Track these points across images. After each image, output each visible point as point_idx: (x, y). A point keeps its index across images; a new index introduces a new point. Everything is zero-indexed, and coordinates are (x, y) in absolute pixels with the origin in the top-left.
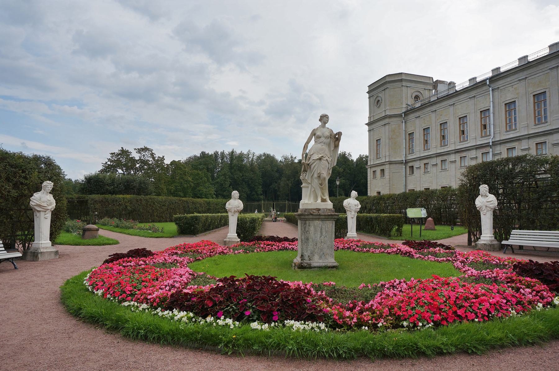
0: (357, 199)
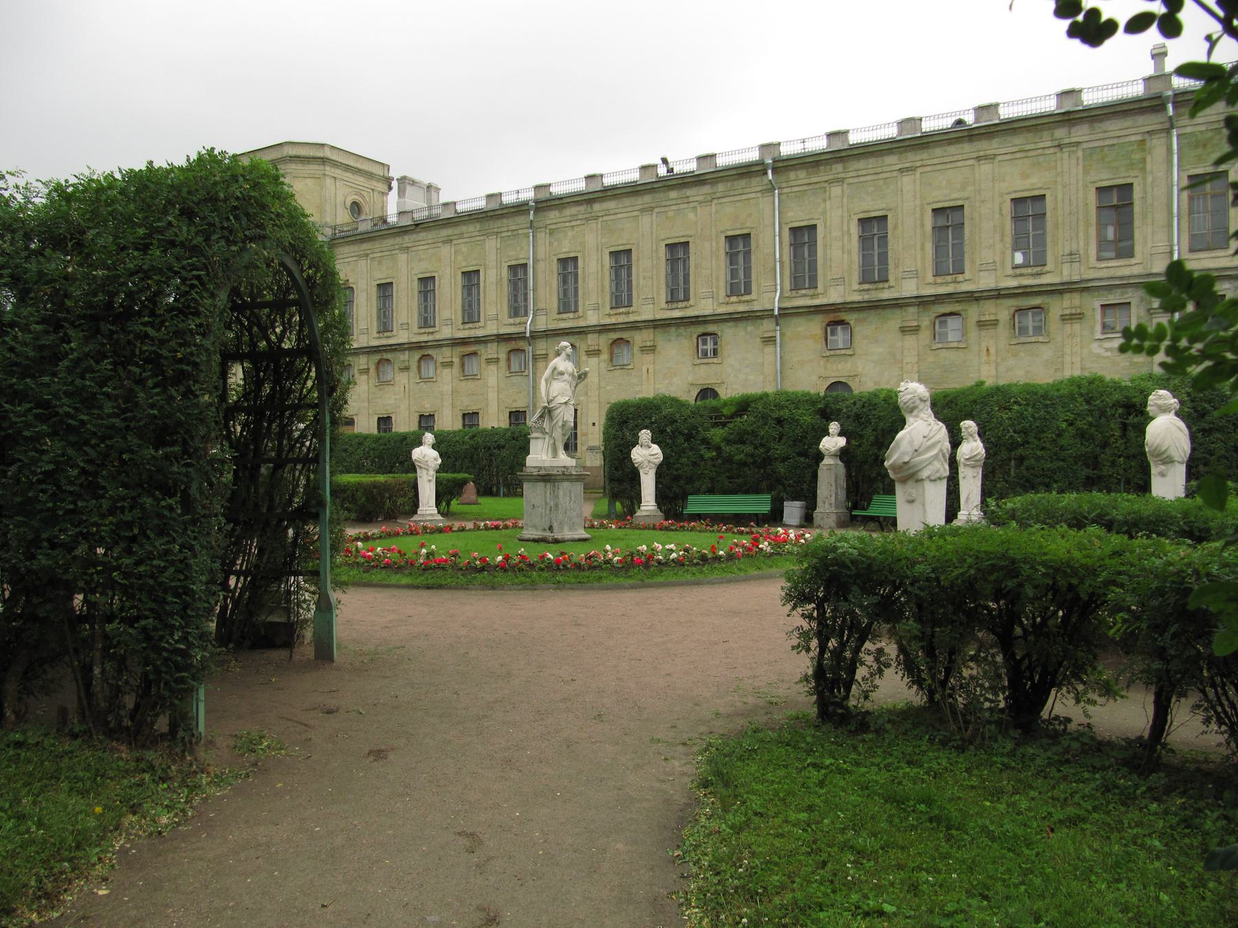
0: (434, 447)
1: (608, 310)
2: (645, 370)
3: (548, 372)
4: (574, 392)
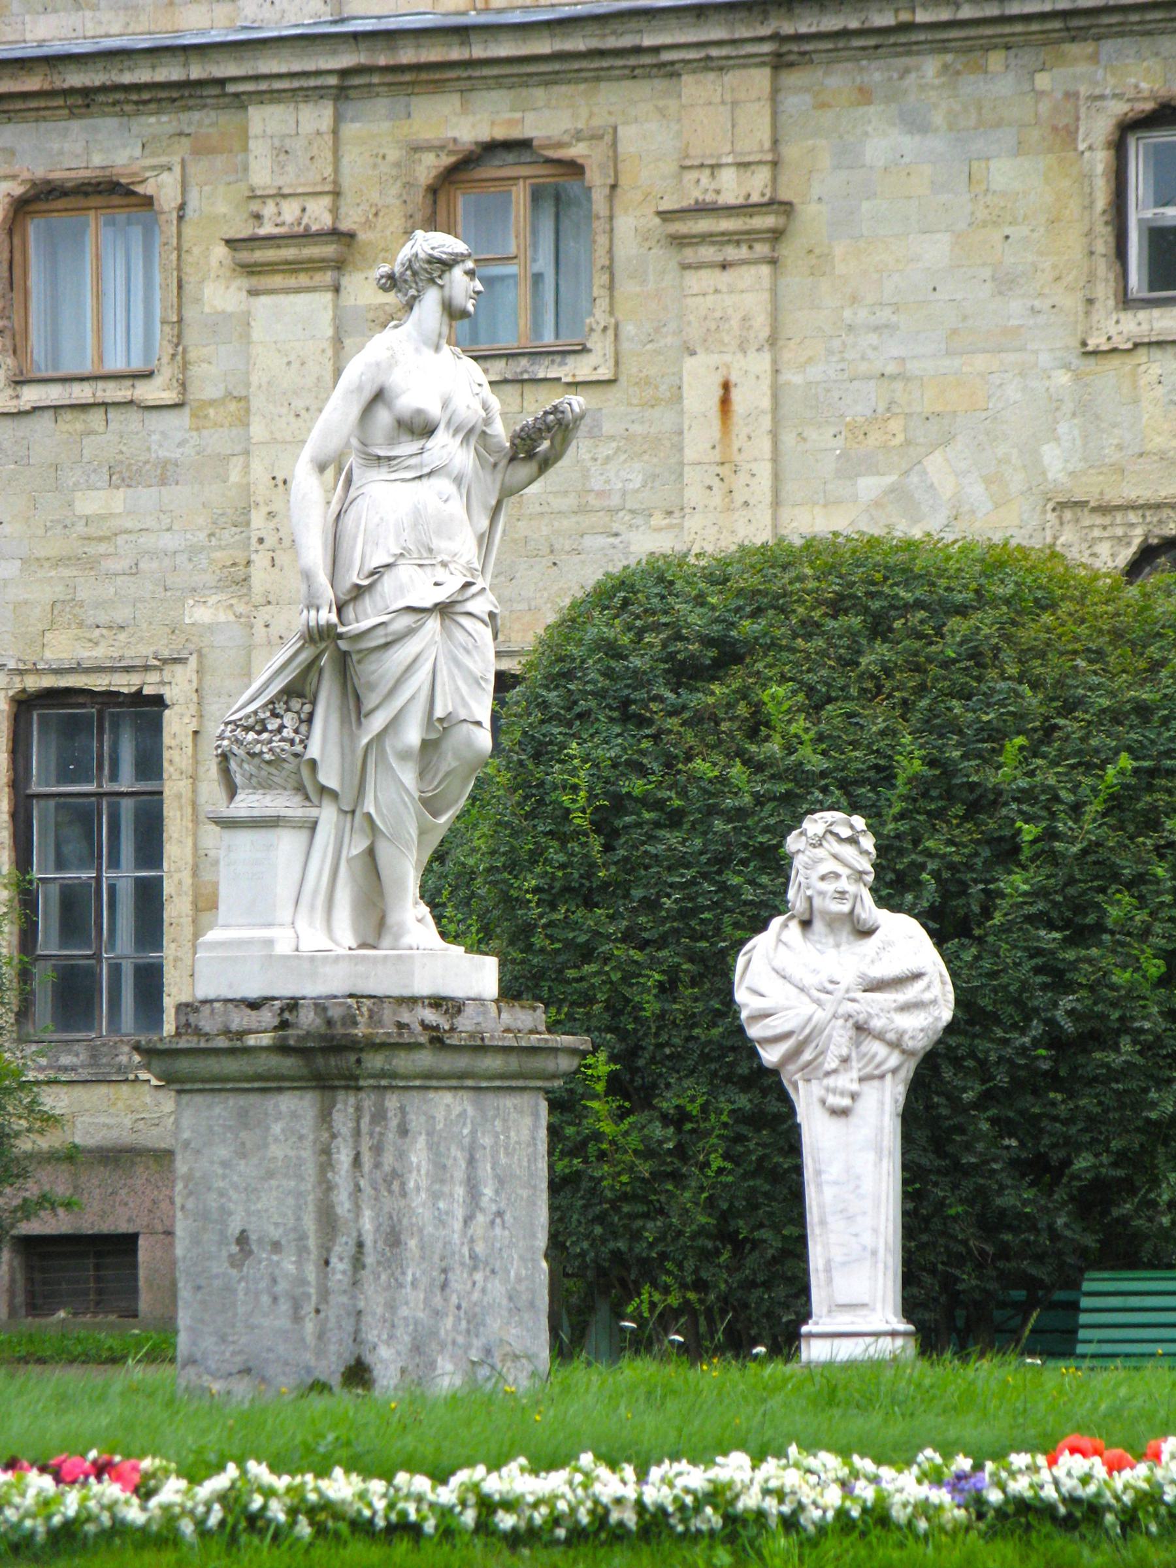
2: (700, 398)
3: (337, 414)
4: (485, 540)
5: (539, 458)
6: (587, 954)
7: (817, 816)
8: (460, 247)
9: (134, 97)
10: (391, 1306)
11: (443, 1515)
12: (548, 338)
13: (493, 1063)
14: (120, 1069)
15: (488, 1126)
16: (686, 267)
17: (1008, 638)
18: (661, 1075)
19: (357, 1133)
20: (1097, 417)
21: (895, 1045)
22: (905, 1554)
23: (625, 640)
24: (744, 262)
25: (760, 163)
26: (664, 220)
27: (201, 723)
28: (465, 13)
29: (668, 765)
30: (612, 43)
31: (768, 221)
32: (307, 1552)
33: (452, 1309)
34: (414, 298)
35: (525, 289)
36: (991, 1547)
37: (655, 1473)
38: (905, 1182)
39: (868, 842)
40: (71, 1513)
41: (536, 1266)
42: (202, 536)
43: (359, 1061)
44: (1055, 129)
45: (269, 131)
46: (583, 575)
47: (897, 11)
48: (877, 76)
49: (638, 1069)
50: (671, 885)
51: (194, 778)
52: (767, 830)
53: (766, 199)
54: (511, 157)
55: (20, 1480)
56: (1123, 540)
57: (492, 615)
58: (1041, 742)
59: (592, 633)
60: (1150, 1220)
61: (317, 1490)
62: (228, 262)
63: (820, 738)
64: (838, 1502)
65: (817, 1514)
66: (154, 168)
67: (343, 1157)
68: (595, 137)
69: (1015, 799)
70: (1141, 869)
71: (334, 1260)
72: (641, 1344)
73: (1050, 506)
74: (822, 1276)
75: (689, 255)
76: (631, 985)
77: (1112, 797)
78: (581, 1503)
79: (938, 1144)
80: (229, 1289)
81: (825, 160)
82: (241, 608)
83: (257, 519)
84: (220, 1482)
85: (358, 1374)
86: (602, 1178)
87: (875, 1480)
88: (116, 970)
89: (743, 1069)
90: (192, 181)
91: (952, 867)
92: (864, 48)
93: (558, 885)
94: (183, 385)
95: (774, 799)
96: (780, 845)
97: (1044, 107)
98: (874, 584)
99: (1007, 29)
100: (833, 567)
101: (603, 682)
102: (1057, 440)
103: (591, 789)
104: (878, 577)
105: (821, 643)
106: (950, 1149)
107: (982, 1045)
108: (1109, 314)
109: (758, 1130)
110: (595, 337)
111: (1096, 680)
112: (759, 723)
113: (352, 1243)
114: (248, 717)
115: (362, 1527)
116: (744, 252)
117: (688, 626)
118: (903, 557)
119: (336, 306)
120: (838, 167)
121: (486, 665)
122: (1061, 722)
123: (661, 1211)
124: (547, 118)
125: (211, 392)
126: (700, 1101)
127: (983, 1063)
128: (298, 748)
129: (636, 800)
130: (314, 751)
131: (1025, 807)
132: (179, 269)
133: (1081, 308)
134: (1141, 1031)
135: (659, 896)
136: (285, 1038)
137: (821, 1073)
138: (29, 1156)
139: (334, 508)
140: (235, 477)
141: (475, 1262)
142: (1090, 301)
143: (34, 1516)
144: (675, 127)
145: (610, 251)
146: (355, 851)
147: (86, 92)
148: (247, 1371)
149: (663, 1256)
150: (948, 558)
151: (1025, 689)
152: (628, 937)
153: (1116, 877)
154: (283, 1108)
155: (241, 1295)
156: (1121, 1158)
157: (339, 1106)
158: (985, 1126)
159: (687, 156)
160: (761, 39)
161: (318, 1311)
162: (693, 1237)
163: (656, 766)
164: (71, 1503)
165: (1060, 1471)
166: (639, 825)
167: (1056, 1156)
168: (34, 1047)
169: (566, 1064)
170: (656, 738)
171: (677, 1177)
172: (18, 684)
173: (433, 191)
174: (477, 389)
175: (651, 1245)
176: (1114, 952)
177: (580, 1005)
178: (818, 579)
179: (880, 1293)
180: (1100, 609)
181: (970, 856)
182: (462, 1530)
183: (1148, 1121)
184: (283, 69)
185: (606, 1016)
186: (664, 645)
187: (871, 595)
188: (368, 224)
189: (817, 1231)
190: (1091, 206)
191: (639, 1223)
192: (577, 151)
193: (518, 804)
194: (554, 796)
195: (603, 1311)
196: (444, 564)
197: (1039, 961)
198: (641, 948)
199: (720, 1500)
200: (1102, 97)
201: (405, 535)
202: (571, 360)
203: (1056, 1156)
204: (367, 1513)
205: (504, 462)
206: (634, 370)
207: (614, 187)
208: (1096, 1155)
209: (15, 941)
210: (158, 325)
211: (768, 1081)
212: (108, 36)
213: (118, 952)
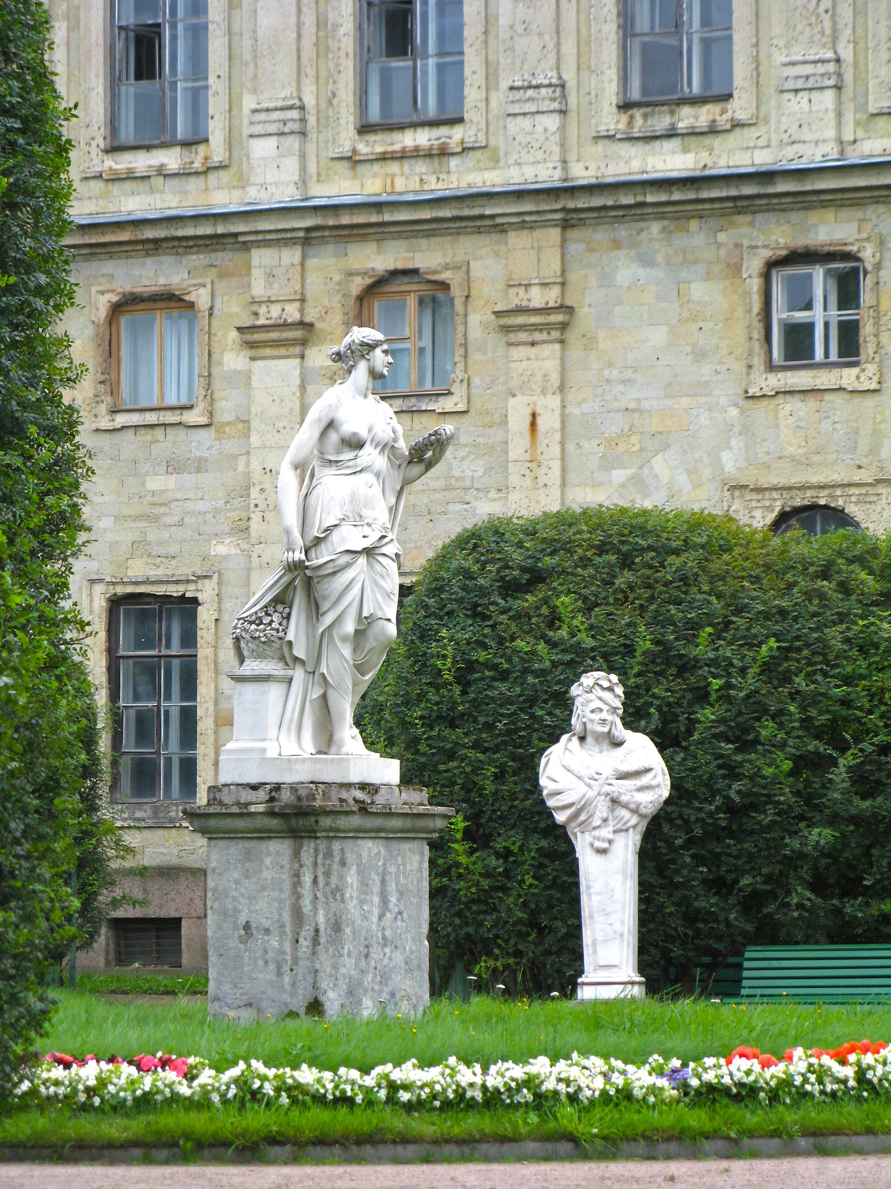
1: (347, 138)
2: (518, 421)
3: (305, 437)
4: (393, 511)
5: (426, 461)
6: (451, 755)
7: (589, 674)
8: (380, 336)
9: (184, 244)
10: (335, 967)
11: (367, 1093)
12: (428, 386)
13: (397, 823)
14: (171, 820)
15: (394, 861)
16: (510, 344)
17: (703, 569)
18: (495, 828)
19: (315, 864)
20: (754, 435)
21: (635, 811)
22: (641, 1116)
23: (475, 568)
24: (545, 342)
25: (554, 283)
26: (497, 317)
27: (220, 615)
28: (379, 195)
29: (501, 643)
30: (466, 212)
31: (559, 318)
32: (286, 1113)
33: (372, 970)
34: (352, 366)
35: (414, 356)
36: (692, 1112)
37: (493, 1069)
38: (640, 892)
39: (619, 690)
40: (147, 1089)
41: (422, 945)
42: (222, 502)
43: (316, 822)
44: (729, 265)
45: (263, 264)
46: (451, 527)
47: (635, 195)
48: (624, 233)
49: (481, 825)
50: (502, 715)
51: (216, 647)
52: (559, 682)
53: (558, 305)
54: (406, 279)
55: (117, 1069)
56: (770, 508)
57: (397, 555)
58: (722, 631)
59: (455, 564)
60: (785, 914)
61: (292, 1077)
62: (238, 340)
63: (591, 628)
64: (602, 1087)
65: (589, 1093)
66: (195, 285)
67: (307, 879)
68: (457, 268)
69: (706, 665)
70: (781, 706)
71: (301, 940)
72: (481, 987)
73: (726, 487)
74: (590, 948)
75: (512, 337)
76: (478, 775)
77: (765, 663)
78: (449, 1086)
79: (661, 871)
80: (239, 956)
81: (593, 282)
82: (244, 546)
83: (254, 493)
84: (235, 1072)
85: (315, 1007)
86: (460, 890)
87: (624, 1073)
88: (168, 761)
89: (543, 825)
90: (217, 293)
91: (669, 705)
92: (616, 217)
93: (434, 715)
94: (211, 413)
95: (563, 664)
96: (567, 692)
97: (723, 252)
98: (624, 536)
99: (701, 207)
100: (599, 525)
101: (462, 594)
102: (730, 448)
103: (454, 657)
104: (626, 531)
105: (592, 571)
106: (667, 873)
107: (686, 811)
108: (761, 374)
109: (553, 861)
110: (456, 385)
111: (756, 594)
112: (555, 618)
113: (312, 929)
114: (251, 615)
115: (319, 1099)
116: (544, 336)
117: (513, 560)
118: (641, 520)
119: (302, 367)
120: (600, 286)
121: (393, 583)
122: (734, 619)
123: (495, 909)
124: (428, 257)
125: (228, 417)
126: (519, 844)
127: (687, 822)
128: (281, 634)
129: (481, 664)
130: (290, 636)
131: (712, 670)
132: (209, 345)
133: (744, 371)
134: (779, 803)
135: (494, 722)
136: (273, 807)
137: (590, 828)
138: (117, 871)
139: (304, 491)
140: (241, 467)
141: (385, 941)
142: (750, 367)
143: (125, 1090)
144: (504, 262)
145: (465, 335)
146: (315, 696)
147: (156, 241)
148: (250, 1005)
149: (497, 936)
150: (668, 521)
151: (713, 599)
152: (476, 746)
153: (766, 711)
154: (271, 849)
155: (246, 960)
156: (768, 879)
157: (305, 848)
158: (688, 860)
159: (511, 279)
160: (555, 211)
161: (292, 970)
162: (514, 925)
163: (493, 644)
164: (148, 1082)
165: (733, 1067)
166: (483, 679)
167: (729, 878)
168: (120, 807)
169: (440, 823)
170: (493, 627)
171: (504, 889)
172: (112, 590)
173: (360, 299)
174: (389, 421)
175: (489, 930)
176: (764, 756)
177: (447, 787)
178: (590, 532)
179: (625, 959)
180: (758, 551)
181: (679, 699)
182: (378, 1102)
183: (785, 856)
184: (272, 227)
185: (462, 793)
186: (498, 572)
187: (622, 542)
188: (322, 319)
189: (588, 922)
190: (749, 311)
191: (482, 917)
192: (446, 276)
193: (411, 666)
194: (432, 661)
195: (460, 968)
196: (369, 525)
197: (720, 761)
198: (484, 753)
199: (532, 1085)
200: (756, 247)
201: (346, 508)
202: (441, 399)
203: (729, 878)
204: (322, 1091)
205: (405, 464)
206: (479, 406)
207: (467, 297)
208: (754, 877)
209: (109, 743)
210: (196, 377)
211: (558, 832)
212: (169, 208)
213: (170, 750)
